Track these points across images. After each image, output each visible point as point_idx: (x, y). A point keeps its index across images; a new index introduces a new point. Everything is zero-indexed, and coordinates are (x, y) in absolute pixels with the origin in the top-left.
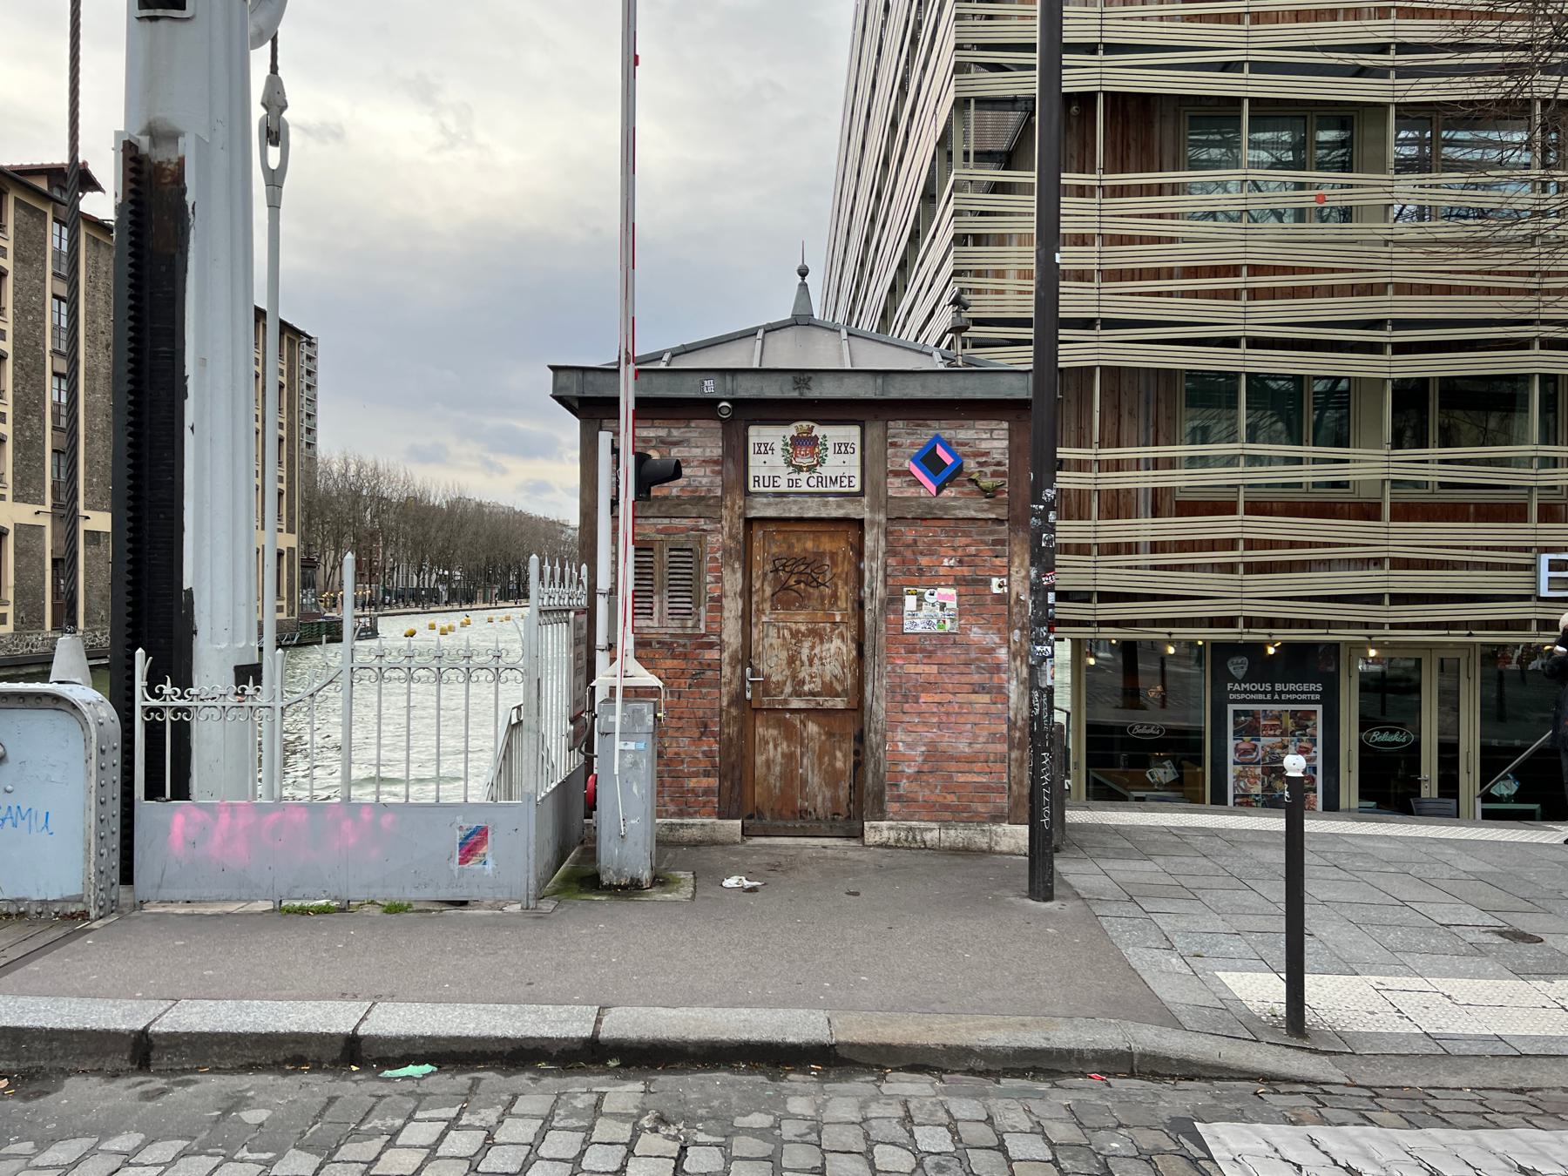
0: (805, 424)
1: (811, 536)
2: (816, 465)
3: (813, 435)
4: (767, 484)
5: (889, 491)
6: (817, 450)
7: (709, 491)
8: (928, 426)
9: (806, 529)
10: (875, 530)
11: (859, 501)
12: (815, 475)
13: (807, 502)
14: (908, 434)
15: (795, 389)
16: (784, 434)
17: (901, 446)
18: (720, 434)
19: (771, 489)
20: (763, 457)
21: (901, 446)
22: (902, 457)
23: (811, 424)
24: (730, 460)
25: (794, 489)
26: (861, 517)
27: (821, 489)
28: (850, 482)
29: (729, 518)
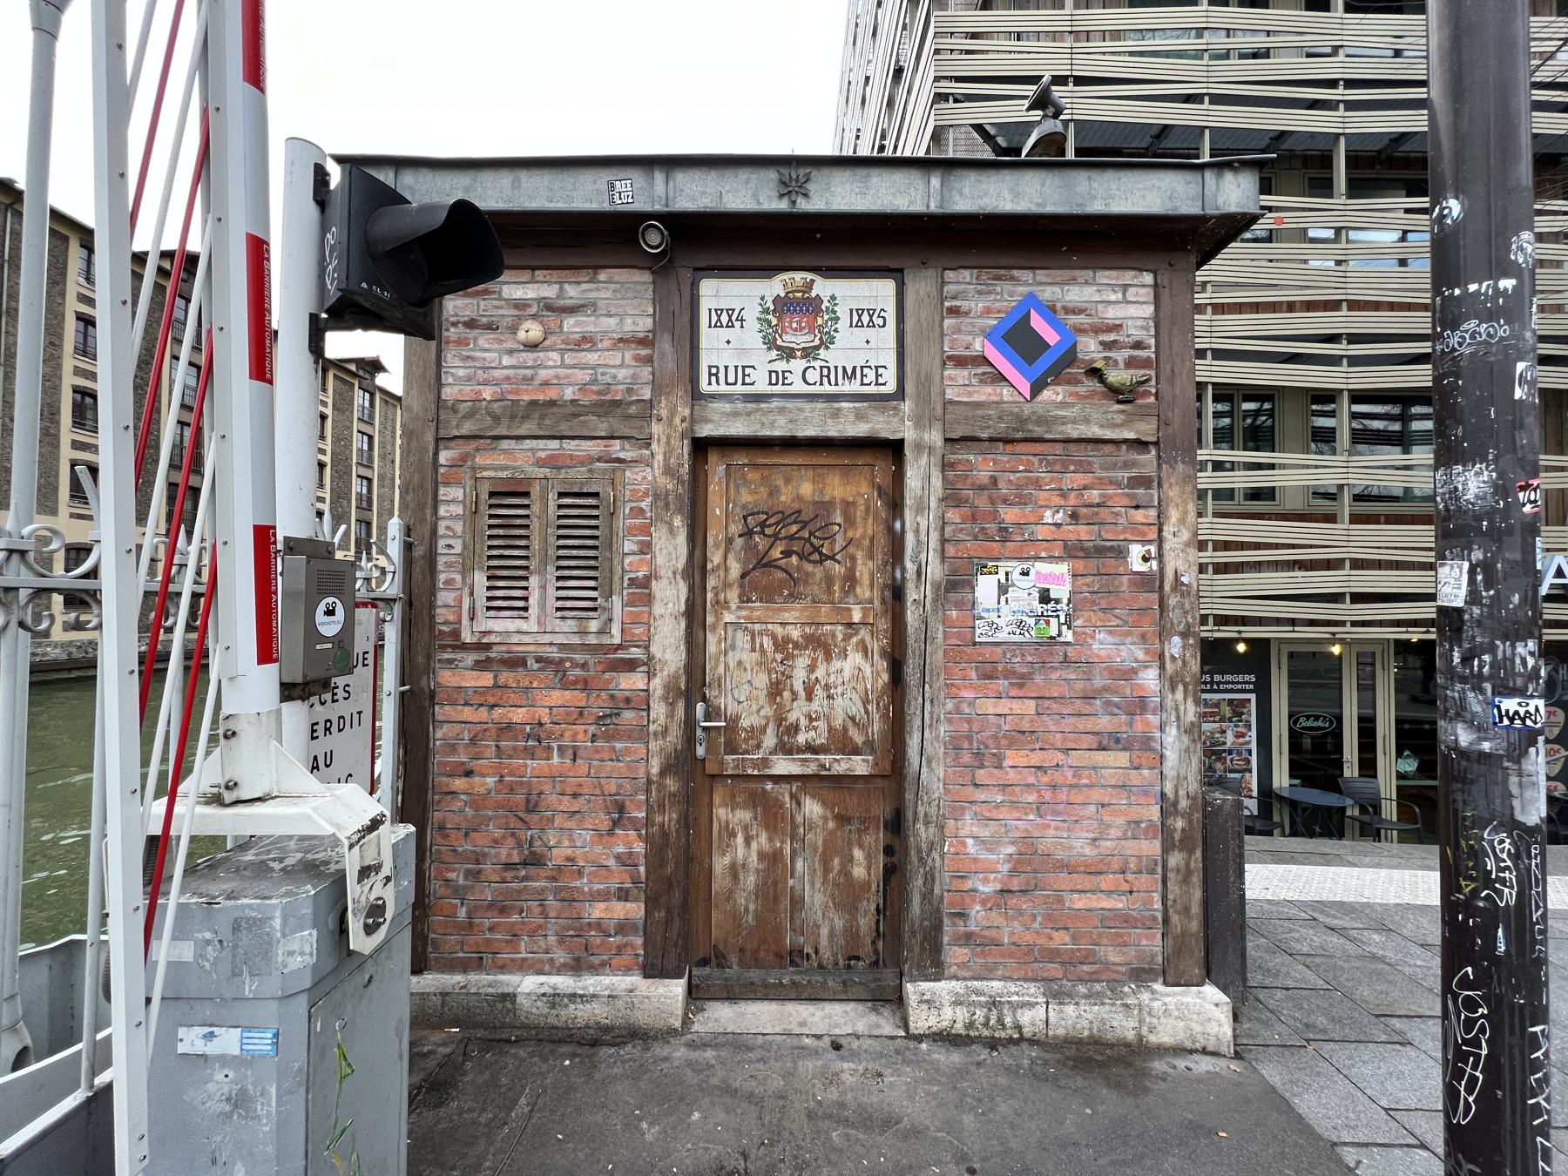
0: (799, 277)
1: (810, 473)
2: (817, 348)
3: (813, 294)
4: (731, 379)
5: (948, 391)
6: (820, 321)
7: (630, 391)
8: (1012, 278)
9: (800, 461)
10: (924, 460)
11: (895, 408)
12: (817, 364)
13: (801, 410)
14: (980, 293)
15: (782, 196)
16: (760, 294)
17: (967, 314)
18: (650, 294)
19: (739, 388)
20: (724, 333)
21: (967, 314)
22: (970, 333)
23: (809, 276)
24: (667, 336)
25: (779, 389)
26: (898, 436)
27: (827, 389)
28: (878, 376)
29: (664, 439)
